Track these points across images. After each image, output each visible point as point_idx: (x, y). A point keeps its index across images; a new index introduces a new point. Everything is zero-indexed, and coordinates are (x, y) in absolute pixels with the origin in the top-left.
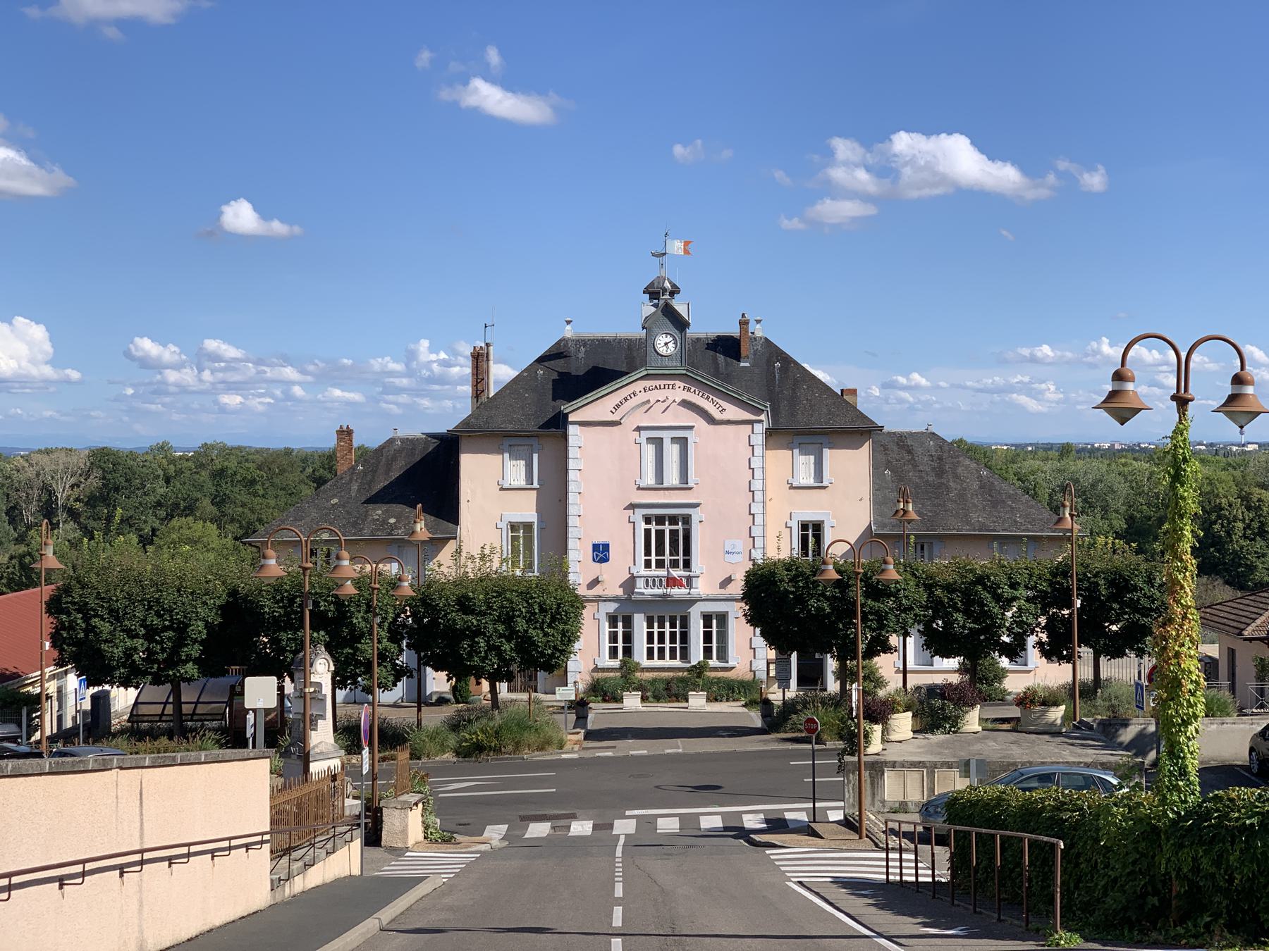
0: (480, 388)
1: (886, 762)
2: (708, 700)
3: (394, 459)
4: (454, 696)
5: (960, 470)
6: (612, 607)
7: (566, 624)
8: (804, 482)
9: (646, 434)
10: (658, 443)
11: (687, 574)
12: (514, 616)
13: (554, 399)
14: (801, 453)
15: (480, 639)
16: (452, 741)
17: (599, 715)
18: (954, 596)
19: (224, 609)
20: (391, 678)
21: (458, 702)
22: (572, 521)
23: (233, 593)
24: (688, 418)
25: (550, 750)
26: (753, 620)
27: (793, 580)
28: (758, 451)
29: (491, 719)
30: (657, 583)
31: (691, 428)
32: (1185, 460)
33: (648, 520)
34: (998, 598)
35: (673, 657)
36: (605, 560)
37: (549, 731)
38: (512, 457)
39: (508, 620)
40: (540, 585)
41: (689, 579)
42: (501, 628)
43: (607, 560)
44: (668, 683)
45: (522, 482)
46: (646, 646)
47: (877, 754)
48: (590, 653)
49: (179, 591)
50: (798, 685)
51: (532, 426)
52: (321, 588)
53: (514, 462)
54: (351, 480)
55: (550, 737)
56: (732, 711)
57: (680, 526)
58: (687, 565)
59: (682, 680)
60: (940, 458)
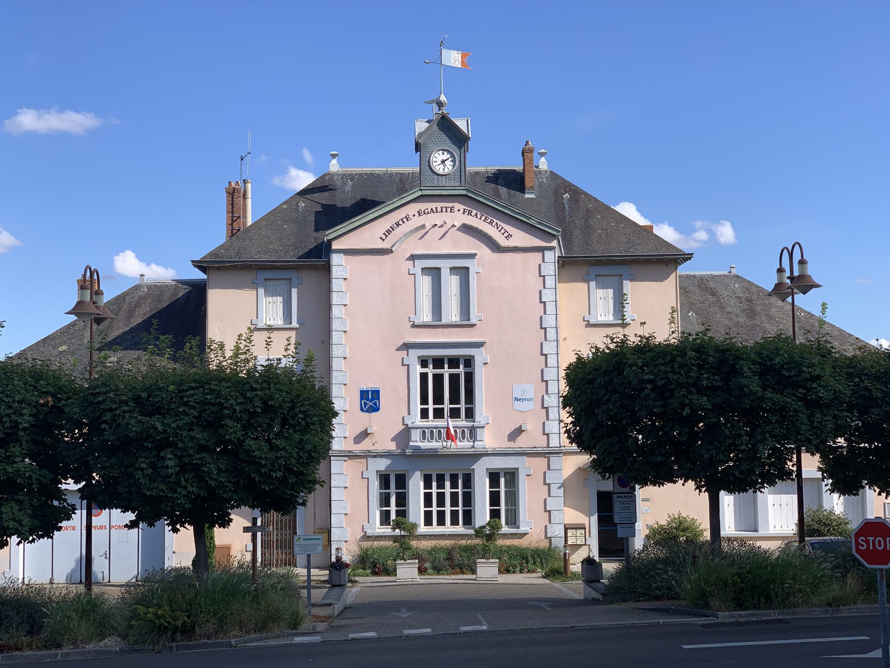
3: (138, 305)
5: (773, 311)
6: (383, 464)
8: (602, 319)
9: (421, 264)
10: (435, 273)
15: (168, 454)
28: (550, 282)
30: (436, 434)
31: (472, 256)
33: (424, 363)
35: (455, 522)
38: (268, 293)
39: (213, 424)
41: (473, 431)
44: (450, 554)
45: (279, 322)
46: (423, 509)
53: (270, 299)
57: (461, 370)
58: (470, 414)
60: (749, 300)
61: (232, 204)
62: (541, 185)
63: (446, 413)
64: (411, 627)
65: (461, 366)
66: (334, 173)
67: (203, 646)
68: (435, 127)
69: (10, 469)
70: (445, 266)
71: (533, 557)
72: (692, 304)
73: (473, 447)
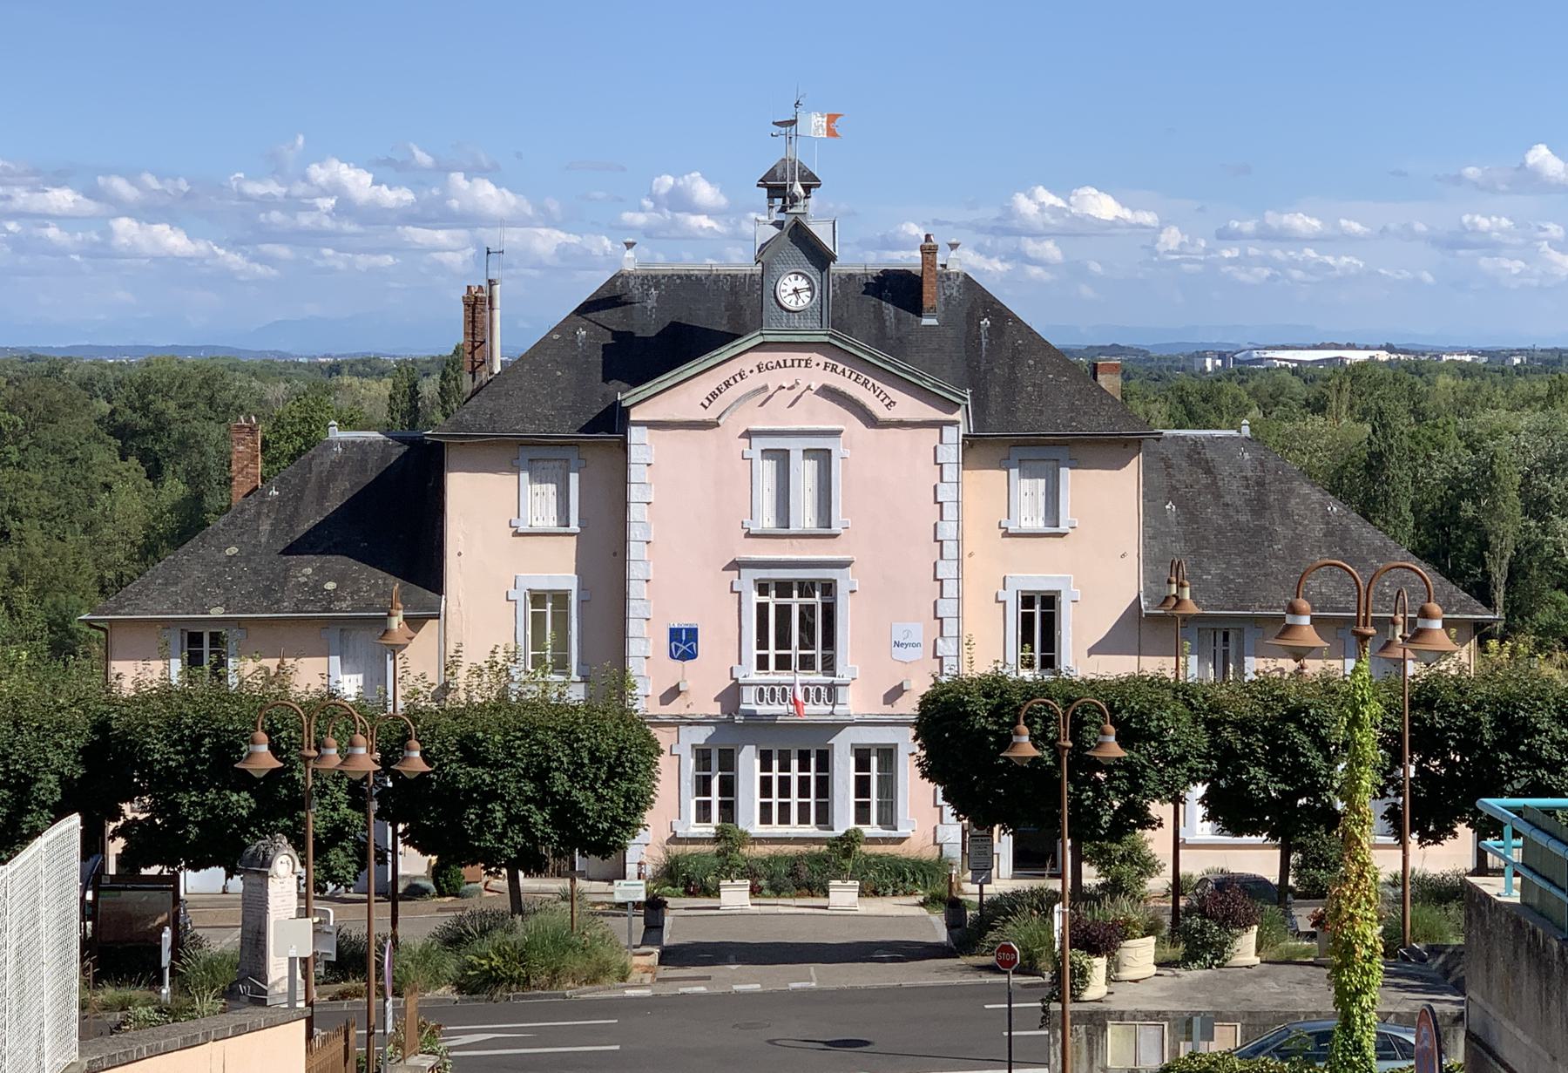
0: (478, 358)
1: (1110, 1013)
2: (863, 893)
3: (331, 476)
4: (436, 883)
6: (701, 735)
7: (631, 781)
9: (760, 444)
10: (781, 458)
11: (829, 679)
12: (549, 769)
13: (606, 379)
14: (1023, 476)
16: (451, 966)
17: (684, 919)
18: (1252, 740)
19: (88, 754)
20: (353, 868)
21: (441, 894)
22: (635, 589)
23: (102, 727)
24: (830, 416)
25: (606, 981)
26: (932, 771)
27: (996, 712)
28: (950, 473)
29: (510, 931)
30: (778, 694)
32: (1364, 702)
33: (763, 589)
34: (1322, 744)
36: (690, 655)
37: (605, 953)
39: (541, 775)
40: (591, 714)
41: (832, 688)
42: (529, 787)
43: (694, 656)
44: (795, 861)
45: (551, 523)
46: (758, 800)
47: (1099, 1001)
48: (671, 816)
49: (16, 724)
50: (1015, 868)
51: (568, 430)
52: (243, 722)
53: (537, 487)
54: (259, 514)
55: (607, 962)
56: (905, 914)
58: (829, 665)
59: (818, 859)
60: (1261, 483)
61: (473, 321)
62: (948, 299)
63: (795, 661)
64: (741, 982)
65: (818, 594)
66: (630, 274)
67: (538, 996)
68: (785, 236)
69: (336, 816)
70: (796, 446)
71: (913, 874)
72: (1175, 489)
73: (832, 713)
